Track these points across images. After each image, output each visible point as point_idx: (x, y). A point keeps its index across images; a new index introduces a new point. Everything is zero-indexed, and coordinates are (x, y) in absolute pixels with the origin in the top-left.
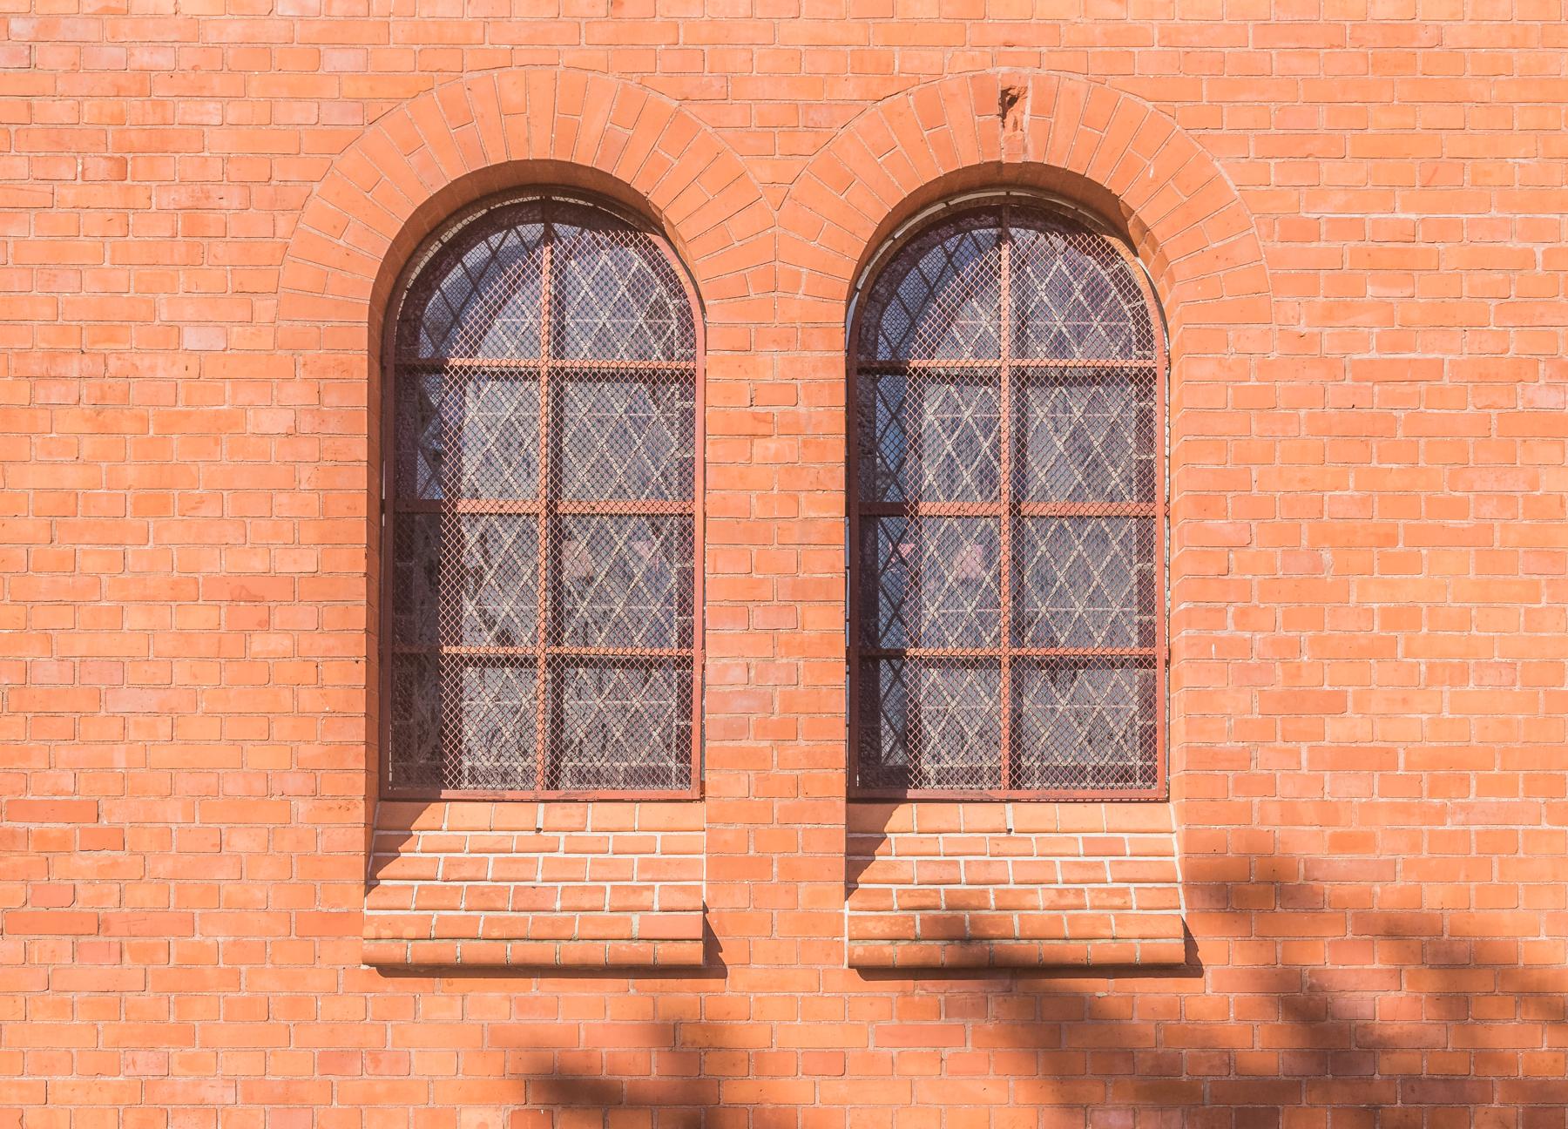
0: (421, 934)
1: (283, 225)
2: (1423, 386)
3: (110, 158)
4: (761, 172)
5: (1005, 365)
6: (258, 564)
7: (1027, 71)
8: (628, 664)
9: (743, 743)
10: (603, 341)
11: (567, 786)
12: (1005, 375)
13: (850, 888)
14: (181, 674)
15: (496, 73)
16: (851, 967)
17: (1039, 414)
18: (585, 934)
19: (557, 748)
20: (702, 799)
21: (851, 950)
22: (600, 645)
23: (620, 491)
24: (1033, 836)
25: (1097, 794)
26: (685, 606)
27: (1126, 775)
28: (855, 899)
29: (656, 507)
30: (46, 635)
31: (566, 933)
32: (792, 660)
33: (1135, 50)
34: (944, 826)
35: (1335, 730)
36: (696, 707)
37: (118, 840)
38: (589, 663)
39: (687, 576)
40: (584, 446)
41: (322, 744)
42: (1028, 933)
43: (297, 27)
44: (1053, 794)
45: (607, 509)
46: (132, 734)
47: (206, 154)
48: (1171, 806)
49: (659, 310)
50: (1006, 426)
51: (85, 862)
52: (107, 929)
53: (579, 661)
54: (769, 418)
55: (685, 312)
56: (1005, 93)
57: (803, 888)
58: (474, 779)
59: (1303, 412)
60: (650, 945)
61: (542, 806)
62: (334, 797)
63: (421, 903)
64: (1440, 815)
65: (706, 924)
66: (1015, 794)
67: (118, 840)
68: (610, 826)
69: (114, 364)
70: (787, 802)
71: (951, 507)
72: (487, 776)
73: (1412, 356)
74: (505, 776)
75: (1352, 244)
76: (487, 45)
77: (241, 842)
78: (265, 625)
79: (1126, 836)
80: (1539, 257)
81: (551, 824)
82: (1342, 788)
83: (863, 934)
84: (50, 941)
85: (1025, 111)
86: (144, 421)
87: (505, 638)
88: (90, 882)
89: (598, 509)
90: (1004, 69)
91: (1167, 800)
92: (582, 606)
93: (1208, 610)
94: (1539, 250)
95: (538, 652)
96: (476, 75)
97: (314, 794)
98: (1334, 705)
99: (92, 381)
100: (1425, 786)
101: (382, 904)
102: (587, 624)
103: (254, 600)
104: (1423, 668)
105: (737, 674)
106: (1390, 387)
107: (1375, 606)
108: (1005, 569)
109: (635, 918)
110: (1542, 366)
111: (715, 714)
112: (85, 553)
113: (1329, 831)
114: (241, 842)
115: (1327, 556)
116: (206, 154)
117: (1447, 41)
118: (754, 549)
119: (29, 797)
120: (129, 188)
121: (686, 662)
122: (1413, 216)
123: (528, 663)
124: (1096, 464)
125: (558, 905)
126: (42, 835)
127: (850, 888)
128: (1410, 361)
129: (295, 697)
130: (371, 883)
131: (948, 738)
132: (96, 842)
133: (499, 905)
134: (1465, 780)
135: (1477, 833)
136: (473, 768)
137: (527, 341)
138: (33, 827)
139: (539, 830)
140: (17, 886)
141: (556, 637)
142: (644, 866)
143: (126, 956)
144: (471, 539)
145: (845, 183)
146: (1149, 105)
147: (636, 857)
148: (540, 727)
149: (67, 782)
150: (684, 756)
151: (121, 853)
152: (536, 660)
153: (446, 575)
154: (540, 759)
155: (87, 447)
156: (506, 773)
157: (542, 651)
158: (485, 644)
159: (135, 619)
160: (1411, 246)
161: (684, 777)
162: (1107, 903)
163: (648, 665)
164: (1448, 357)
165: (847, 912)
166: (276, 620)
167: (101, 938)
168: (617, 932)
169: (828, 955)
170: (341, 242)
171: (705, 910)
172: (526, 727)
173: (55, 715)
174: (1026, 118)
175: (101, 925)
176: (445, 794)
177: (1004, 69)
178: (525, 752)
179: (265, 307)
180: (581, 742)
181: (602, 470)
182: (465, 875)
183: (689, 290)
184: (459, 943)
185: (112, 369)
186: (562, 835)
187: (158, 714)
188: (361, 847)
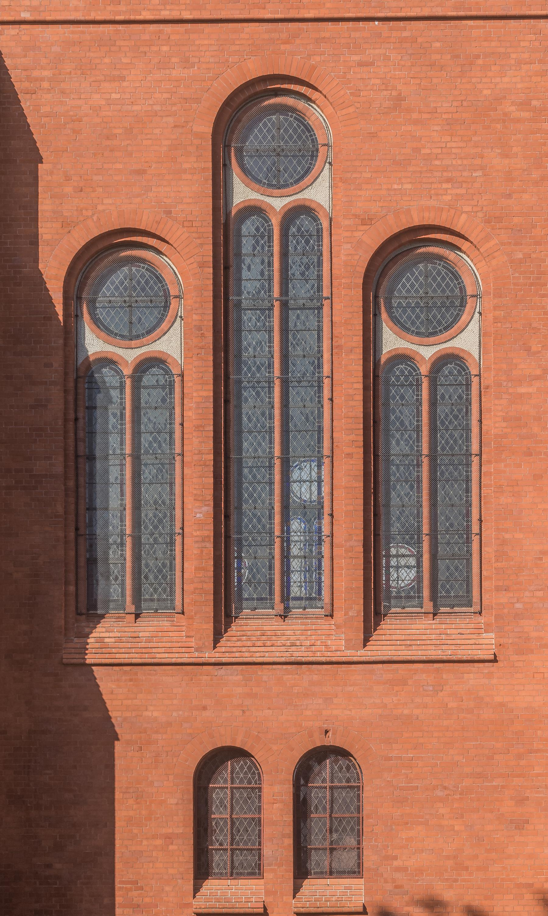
0: (205, 907)
1: (175, 760)
2: (414, 791)
3: (139, 746)
4: (275, 748)
5: (328, 785)
6: (170, 831)
7: (330, 726)
8: (247, 850)
9: (272, 867)
10: (241, 781)
11: (234, 876)
12: (328, 787)
13: (294, 897)
14: (154, 854)
15: (219, 727)
16: (294, 913)
17: (336, 794)
18: (239, 907)
19: (233, 867)
20: (263, 879)
21: (294, 910)
22: (241, 846)
23: (245, 813)
24: (333, 886)
25: (348, 877)
26: (260, 837)
27: (354, 872)
28: (295, 899)
29: (253, 816)
30: (126, 846)
31: (235, 907)
32: (282, 850)
33: (353, 721)
34: (315, 884)
35: (396, 863)
36: (262, 859)
37: (141, 888)
38: (239, 849)
39: (260, 831)
40: (237, 802)
41: (184, 868)
42: (331, 906)
43: (177, 718)
44: (338, 877)
45: (243, 817)
46: (144, 867)
47: (159, 745)
48: (363, 879)
49: (254, 773)
50: (328, 797)
51: (135, 893)
52: (140, 907)
53: (237, 849)
54: (277, 799)
55: (259, 774)
56: (326, 730)
57: (284, 898)
58: (214, 875)
59: (389, 797)
60: (252, 909)
61: (229, 880)
62: (187, 879)
63: (205, 901)
64: (417, 881)
65: (264, 904)
66: (330, 877)
67: (141, 888)
68: (244, 885)
69: (139, 789)
70: (281, 879)
71: (317, 815)
72: (218, 874)
73: (412, 785)
74: (221, 874)
75: (399, 761)
76: (217, 722)
77: (167, 888)
78: (172, 844)
79: (353, 886)
80: (438, 764)
81: (231, 884)
82: (398, 875)
83: (296, 907)
84: (128, 909)
85: (330, 734)
86: (146, 801)
87: (221, 844)
88: (136, 897)
89: (241, 816)
90: (326, 726)
91: (363, 878)
92: (237, 837)
93: (369, 839)
94: (439, 762)
95: (228, 848)
96: (215, 728)
97: (183, 878)
98: (395, 858)
99: (135, 793)
100: (414, 875)
101: (197, 901)
102: (238, 841)
103: (169, 838)
104: (414, 850)
105: (270, 853)
106: (407, 791)
107: (404, 837)
108: (328, 829)
109: (249, 904)
110: (439, 787)
111: (265, 861)
112: (134, 829)
113: (394, 884)
114: (167, 888)
115: (394, 827)
116: (159, 745)
117: (419, 718)
118: (274, 827)
119: (123, 880)
120: (142, 753)
121: (260, 849)
122: (412, 755)
123: (226, 850)
124: (348, 805)
125: (233, 901)
126: (126, 888)
127: (294, 897)
128: (411, 786)
129: (178, 858)
130: (194, 897)
131: (316, 865)
132: (138, 889)
133: (221, 901)
134: (423, 874)
135: (425, 884)
136: (214, 872)
137: (226, 781)
138: (124, 886)
139: (229, 886)
140: (121, 898)
141: (232, 845)
142: (251, 893)
143: (144, 912)
144: (214, 823)
145: (292, 750)
146: (356, 733)
147: (249, 891)
148: (229, 864)
149: (131, 876)
150: (259, 869)
151: (142, 891)
152: (228, 849)
153: (209, 830)
154: (229, 870)
155: (135, 807)
156: (222, 873)
157: (229, 847)
158: (217, 846)
159: (145, 843)
160: (411, 762)
161: (259, 874)
162: (348, 900)
163: (252, 850)
164: (419, 785)
165: (293, 902)
166: (174, 842)
167: (138, 909)
168: (246, 907)
169: (289, 911)
170: (187, 763)
171: (264, 902)
172: (226, 863)
173: (129, 863)
174: (331, 735)
175: (138, 906)
176: (309, 877)
177: (326, 726)
178: (225, 869)
179: (171, 777)
180: (237, 866)
181: (242, 808)
182: (213, 895)
183: (260, 770)
184: (213, 909)
185: (139, 791)
186: (234, 887)
187: (150, 862)
188: (192, 889)
